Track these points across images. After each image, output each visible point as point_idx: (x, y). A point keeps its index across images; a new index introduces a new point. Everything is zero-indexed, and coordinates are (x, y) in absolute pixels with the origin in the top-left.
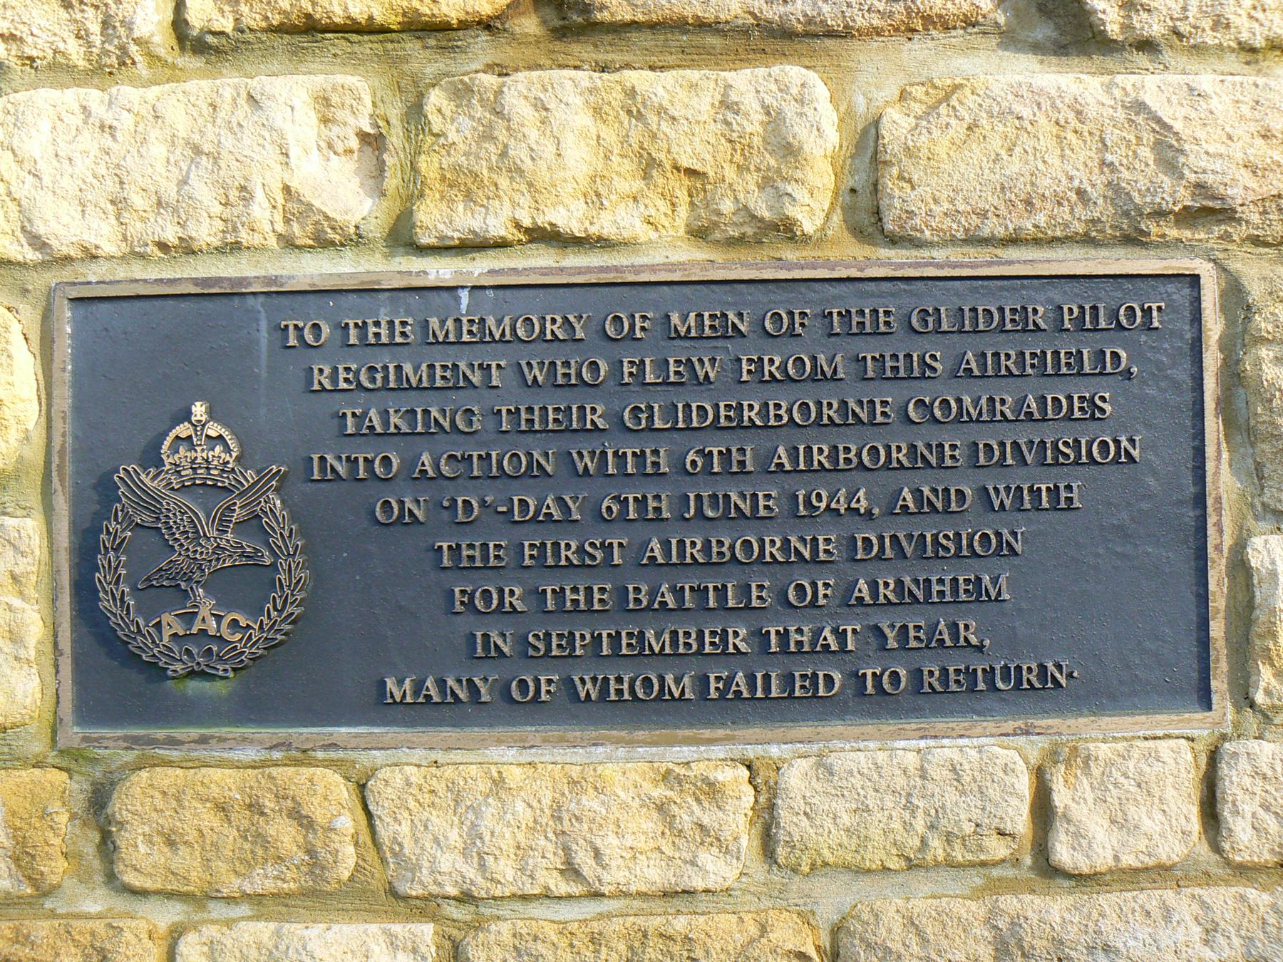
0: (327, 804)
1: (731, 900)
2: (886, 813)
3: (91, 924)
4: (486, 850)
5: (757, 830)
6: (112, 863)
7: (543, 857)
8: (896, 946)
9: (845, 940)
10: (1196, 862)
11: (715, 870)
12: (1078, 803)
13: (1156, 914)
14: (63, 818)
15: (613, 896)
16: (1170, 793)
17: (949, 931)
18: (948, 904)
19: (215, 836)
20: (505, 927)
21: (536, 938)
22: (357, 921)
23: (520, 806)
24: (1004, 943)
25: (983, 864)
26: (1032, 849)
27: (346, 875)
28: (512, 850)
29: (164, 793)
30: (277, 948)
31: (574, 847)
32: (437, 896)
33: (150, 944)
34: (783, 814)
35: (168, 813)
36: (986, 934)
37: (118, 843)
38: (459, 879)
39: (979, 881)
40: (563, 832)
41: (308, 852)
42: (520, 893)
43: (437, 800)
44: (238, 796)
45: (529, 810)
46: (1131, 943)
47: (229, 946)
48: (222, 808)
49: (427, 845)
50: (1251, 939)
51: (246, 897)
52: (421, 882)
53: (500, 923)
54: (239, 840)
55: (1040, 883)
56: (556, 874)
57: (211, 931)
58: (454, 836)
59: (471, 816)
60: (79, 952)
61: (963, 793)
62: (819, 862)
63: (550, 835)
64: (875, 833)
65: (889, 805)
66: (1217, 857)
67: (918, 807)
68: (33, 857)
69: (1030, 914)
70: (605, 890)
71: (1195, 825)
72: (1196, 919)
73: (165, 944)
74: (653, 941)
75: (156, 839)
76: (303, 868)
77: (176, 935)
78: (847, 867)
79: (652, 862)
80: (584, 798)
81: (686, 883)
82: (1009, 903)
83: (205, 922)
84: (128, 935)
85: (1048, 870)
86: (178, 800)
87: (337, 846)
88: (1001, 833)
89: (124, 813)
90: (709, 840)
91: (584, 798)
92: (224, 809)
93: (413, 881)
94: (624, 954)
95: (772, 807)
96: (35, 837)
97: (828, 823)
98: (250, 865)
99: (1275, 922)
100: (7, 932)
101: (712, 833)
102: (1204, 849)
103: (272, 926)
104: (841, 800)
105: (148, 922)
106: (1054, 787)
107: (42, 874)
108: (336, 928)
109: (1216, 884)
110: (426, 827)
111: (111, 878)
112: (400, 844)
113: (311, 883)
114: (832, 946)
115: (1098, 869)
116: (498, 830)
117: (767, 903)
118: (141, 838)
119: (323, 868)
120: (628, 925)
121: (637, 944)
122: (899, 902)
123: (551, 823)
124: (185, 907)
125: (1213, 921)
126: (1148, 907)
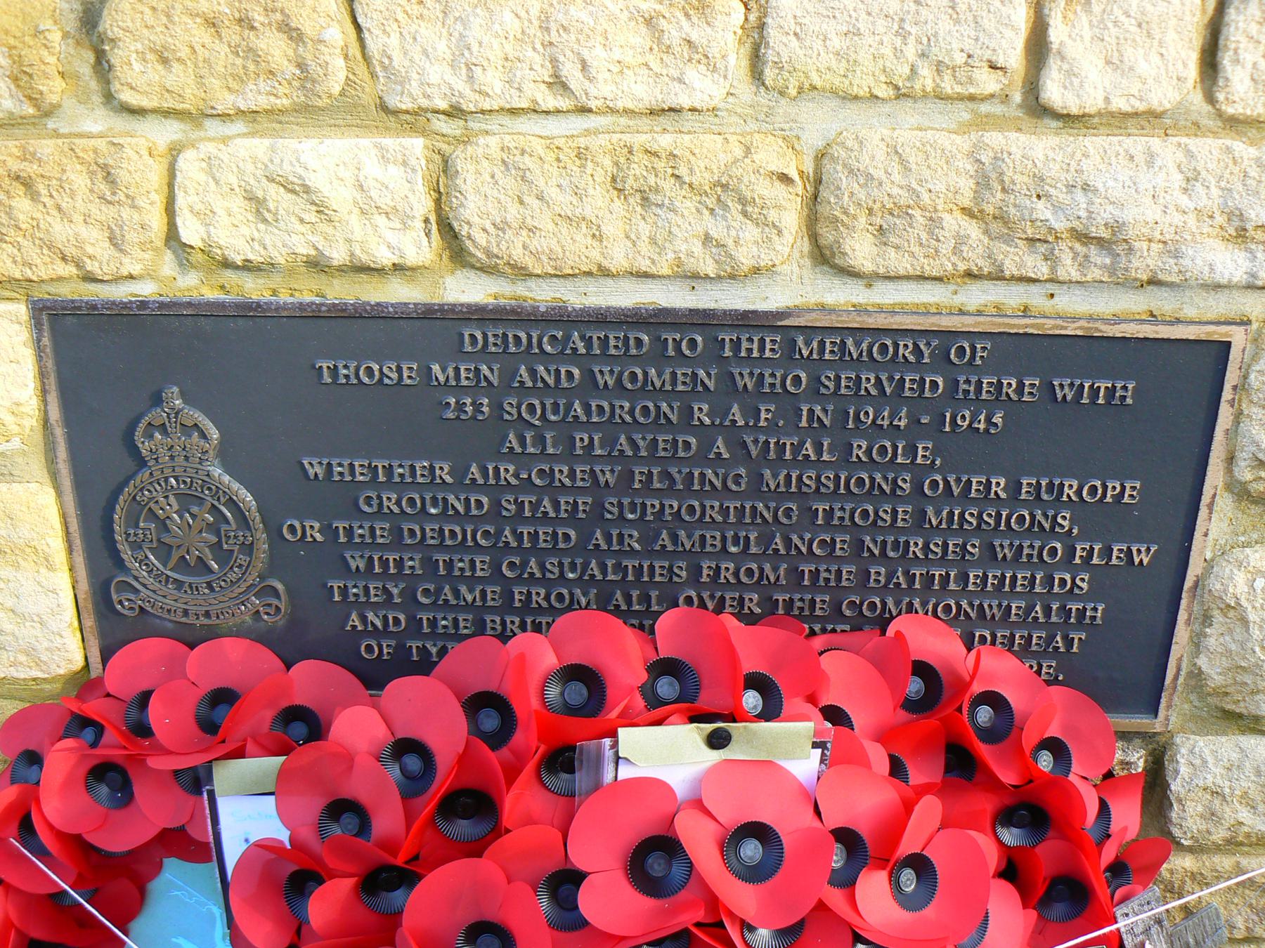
0: (315, 15)
1: (716, 120)
2: (877, 38)
3: (93, 142)
4: (474, 60)
5: (746, 50)
6: (108, 82)
7: (531, 69)
8: (878, 174)
9: (828, 166)
10: (1188, 112)
11: (702, 88)
12: (1075, 40)
13: (1140, 159)
14: (56, 37)
15: (600, 112)
16: (1171, 36)
17: (932, 161)
18: (934, 136)
19: (206, 52)
20: (493, 141)
21: (523, 152)
22: (349, 136)
23: (508, 16)
24: (986, 177)
25: (972, 98)
26: (1023, 87)
27: (336, 90)
28: (501, 63)
29: (154, 9)
30: (272, 161)
31: (561, 58)
32: (426, 110)
33: (151, 161)
34: (773, 34)
35: (159, 29)
36: (969, 167)
37: (113, 61)
38: (448, 92)
39: (966, 116)
40: (551, 43)
41: (299, 66)
42: (508, 106)
43: (425, 12)
44: (227, 11)
45: (517, 20)
46: (1111, 183)
47: (226, 160)
48: (212, 23)
49: (417, 57)
50: (1230, 190)
51: (241, 113)
52: (411, 95)
53: (489, 138)
54: (230, 56)
55: (1028, 122)
56: (543, 86)
57: (209, 148)
58: (442, 48)
59: (459, 27)
60: (84, 169)
61: (957, 22)
62: (807, 86)
63: (539, 46)
64: (864, 57)
65: (881, 30)
66: (1210, 108)
67: (910, 33)
68: (31, 76)
69: (1013, 149)
70: (593, 104)
71: (1192, 71)
72: (1179, 166)
73: (165, 162)
74: (639, 156)
75: (150, 56)
76: (294, 83)
77: (175, 153)
78: (834, 92)
79: (640, 78)
80: (572, 8)
81: (672, 102)
82: (995, 139)
83: (202, 140)
84: (128, 150)
85: (1037, 108)
86: (168, 16)
87: (327, 58)
88: (993, 67)
89: (116, 29)
90: (697, 57)
91: (572, 8)
92: (214, 24)
93: (403, 93)
94: (610, 169)
95: (762, 26)
96: (30, 56)
97: (818, 45)
98: (242, 81)
99: (1256, 175)
100: (15, 151)
101: (700, 50)
102: (1197, 98)
103: (267, 142)
104: (832, 22)
105: (148, 140)
106: (1052, 22)
107: (41, 93)
108: (328, 142)
109: (1204, 136)
110: (415, 39)
111: (109, 97)
112: (389, 58)
113: (303, 98)
114: (815, 173)
115: (1087, 111)
116: (486, 40)
117: (753, 126)
118: (134, 55)
119: (314, 81)
120: (614, 141)
121: (622, 160)
122: (885, 132)
123: (539, 34)
124: (182, 126)
125: (1195, 170)
126: (1132, 151)
